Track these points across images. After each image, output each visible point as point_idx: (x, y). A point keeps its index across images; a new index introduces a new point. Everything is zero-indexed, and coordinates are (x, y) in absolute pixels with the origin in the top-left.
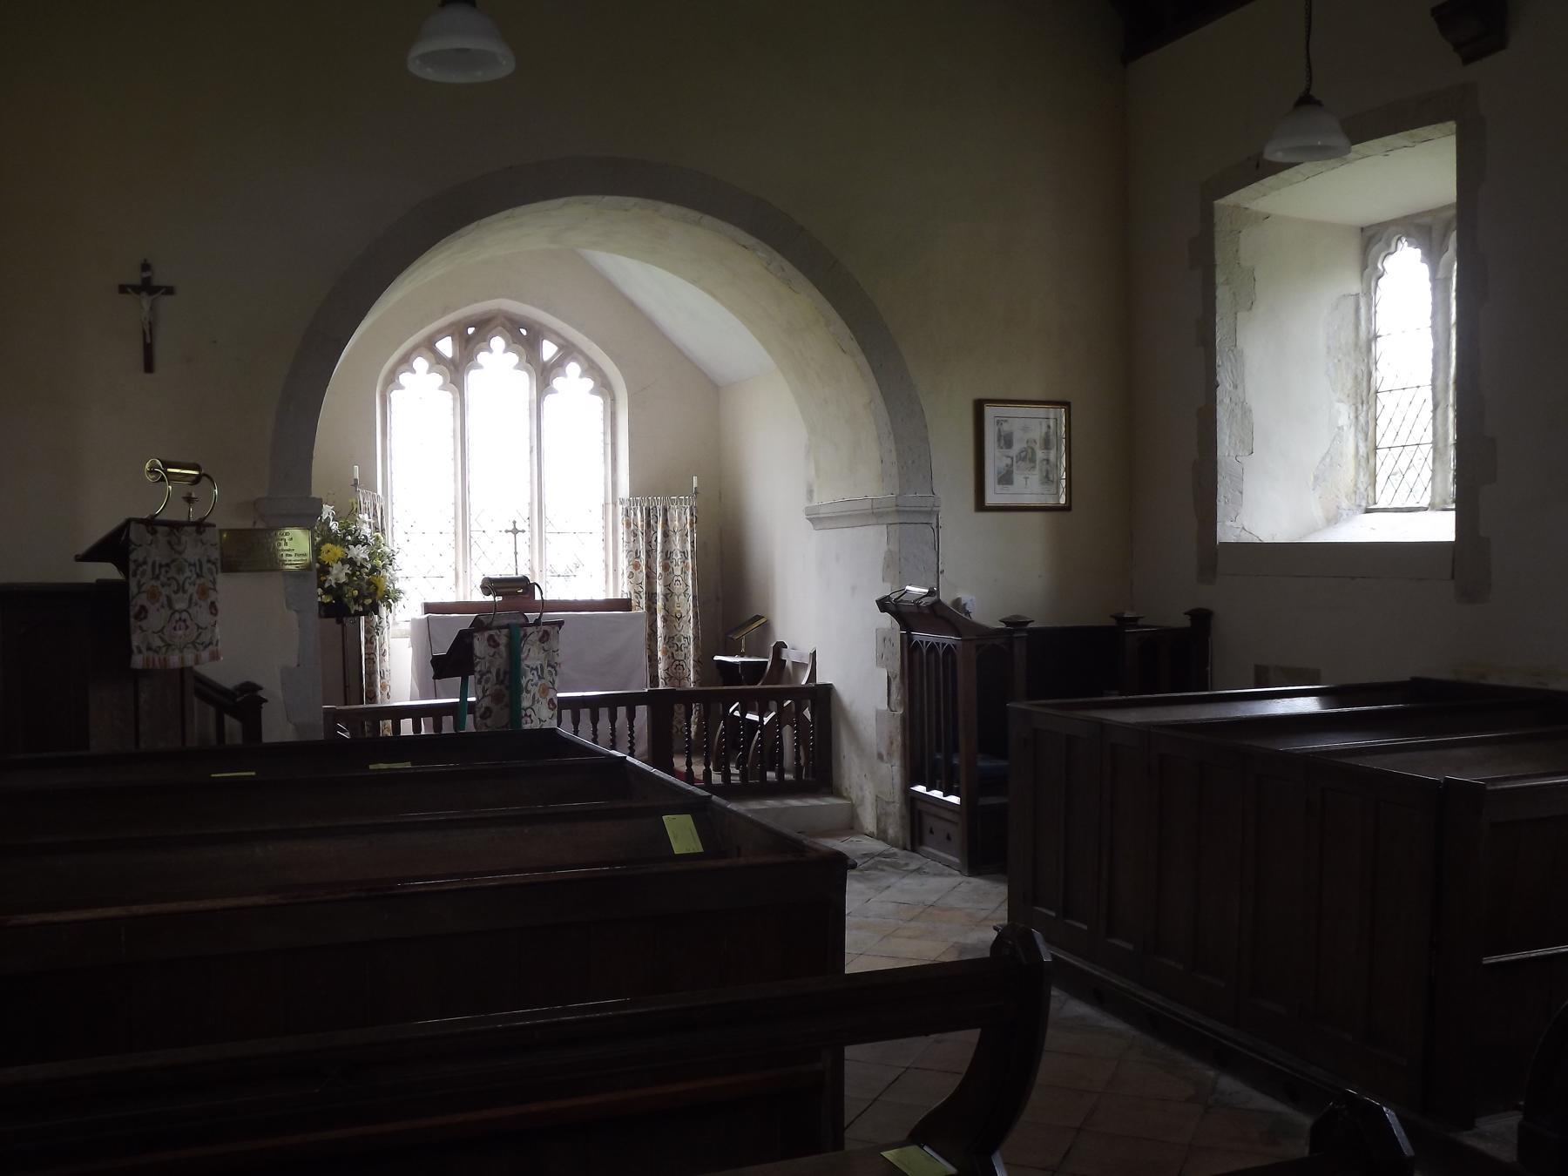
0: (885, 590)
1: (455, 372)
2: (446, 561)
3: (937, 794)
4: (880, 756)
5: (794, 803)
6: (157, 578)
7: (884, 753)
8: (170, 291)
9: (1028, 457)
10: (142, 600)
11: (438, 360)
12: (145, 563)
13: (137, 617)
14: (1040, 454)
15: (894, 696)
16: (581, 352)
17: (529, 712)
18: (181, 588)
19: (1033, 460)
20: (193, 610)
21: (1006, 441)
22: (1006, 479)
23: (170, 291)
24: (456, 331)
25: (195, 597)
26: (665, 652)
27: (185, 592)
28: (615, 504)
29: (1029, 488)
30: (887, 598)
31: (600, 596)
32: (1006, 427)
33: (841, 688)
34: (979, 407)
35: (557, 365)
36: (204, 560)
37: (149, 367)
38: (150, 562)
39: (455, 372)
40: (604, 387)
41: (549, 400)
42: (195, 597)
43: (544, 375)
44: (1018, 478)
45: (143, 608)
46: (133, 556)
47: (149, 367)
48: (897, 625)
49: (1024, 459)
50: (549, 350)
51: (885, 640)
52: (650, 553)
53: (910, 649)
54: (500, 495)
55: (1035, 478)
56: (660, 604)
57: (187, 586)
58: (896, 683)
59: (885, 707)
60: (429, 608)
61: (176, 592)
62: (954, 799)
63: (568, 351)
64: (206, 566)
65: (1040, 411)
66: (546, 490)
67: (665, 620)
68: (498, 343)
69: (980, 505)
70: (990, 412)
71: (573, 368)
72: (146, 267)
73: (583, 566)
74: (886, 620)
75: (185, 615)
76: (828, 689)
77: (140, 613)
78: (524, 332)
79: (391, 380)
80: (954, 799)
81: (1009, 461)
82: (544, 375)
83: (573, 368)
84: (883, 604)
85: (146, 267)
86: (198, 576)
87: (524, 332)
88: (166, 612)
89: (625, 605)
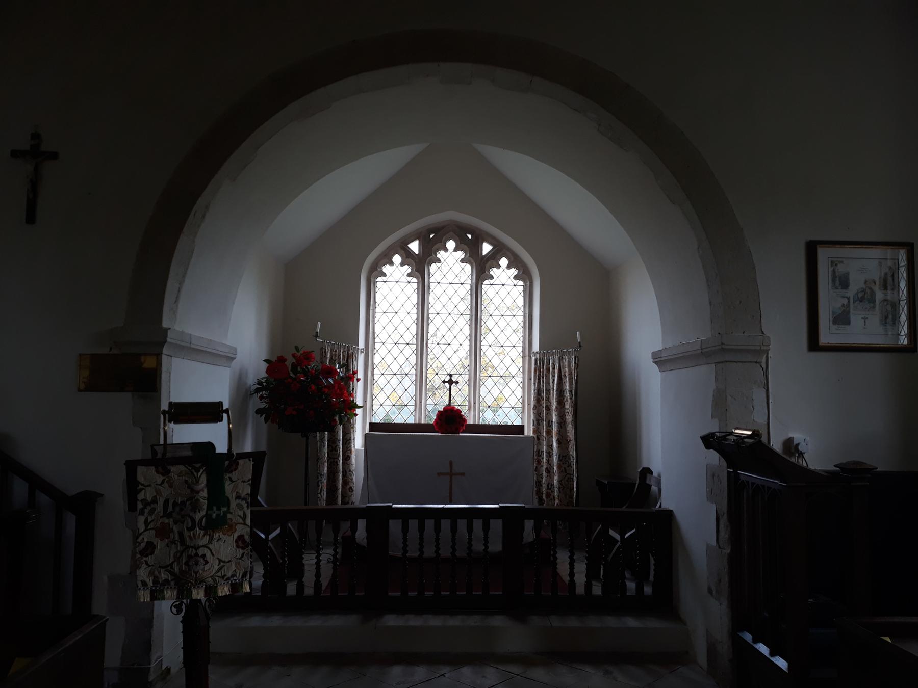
0: (713, 427)
1: (420, 266)
2: (408, 398)
3: (763, 649)
4: (710, 591)
5: (632, 622)
7: (713, 588)
8: (54, 156)
9: (865, 298)
11: (408, 257)
14: (879, 295)
15: (722, 533)
16: (509, 249)
17: (201, 551)
19: (872, 300)
21: (842, 282)
22: (842, 319)
23: (54, 156)
24: (422, 236)
26: (559, 467)
28: (530, 357)
29: (864, 329)
30: (712, 435)
31: (411, 420)
32: (841, 269)
33: (680, 516)
34: (811, 248)
35: (493, 259)
37: (31, 218)
39: (420, 266)
40: (524, 275)
41: (486, 286)
43: (482, 269)
44: (856, 319)
46: (141, 496)
47: (31, 218)
48: (725, 464)
49: (861, 300)
50: (487, 248)
51: (712, 475)
53: (735, 486)
54: (449, 351)
55: (875, 319)
56: (555, 429)
58: (724, 521)
59: (714, 543)
60: (374, 427)
62: (781, 663)
63: (499, 250)
65: (875, 253)
66: (765, 400)
67: (559, 442)
68: (451, 244)
69: (814, 344)
70: (823, 254)
71: (504, 262)
72: (36, 136)
73: (504, 399)
74: (714, 457)
76: (669, 514)
78: (470, 236)
79: (376, 271)
80: (781, 663)
81: (845, 301)
82: (482, 269)
83: (504, 262)
84: (709, 441)
87: (470, 236)
89: (520, 429)
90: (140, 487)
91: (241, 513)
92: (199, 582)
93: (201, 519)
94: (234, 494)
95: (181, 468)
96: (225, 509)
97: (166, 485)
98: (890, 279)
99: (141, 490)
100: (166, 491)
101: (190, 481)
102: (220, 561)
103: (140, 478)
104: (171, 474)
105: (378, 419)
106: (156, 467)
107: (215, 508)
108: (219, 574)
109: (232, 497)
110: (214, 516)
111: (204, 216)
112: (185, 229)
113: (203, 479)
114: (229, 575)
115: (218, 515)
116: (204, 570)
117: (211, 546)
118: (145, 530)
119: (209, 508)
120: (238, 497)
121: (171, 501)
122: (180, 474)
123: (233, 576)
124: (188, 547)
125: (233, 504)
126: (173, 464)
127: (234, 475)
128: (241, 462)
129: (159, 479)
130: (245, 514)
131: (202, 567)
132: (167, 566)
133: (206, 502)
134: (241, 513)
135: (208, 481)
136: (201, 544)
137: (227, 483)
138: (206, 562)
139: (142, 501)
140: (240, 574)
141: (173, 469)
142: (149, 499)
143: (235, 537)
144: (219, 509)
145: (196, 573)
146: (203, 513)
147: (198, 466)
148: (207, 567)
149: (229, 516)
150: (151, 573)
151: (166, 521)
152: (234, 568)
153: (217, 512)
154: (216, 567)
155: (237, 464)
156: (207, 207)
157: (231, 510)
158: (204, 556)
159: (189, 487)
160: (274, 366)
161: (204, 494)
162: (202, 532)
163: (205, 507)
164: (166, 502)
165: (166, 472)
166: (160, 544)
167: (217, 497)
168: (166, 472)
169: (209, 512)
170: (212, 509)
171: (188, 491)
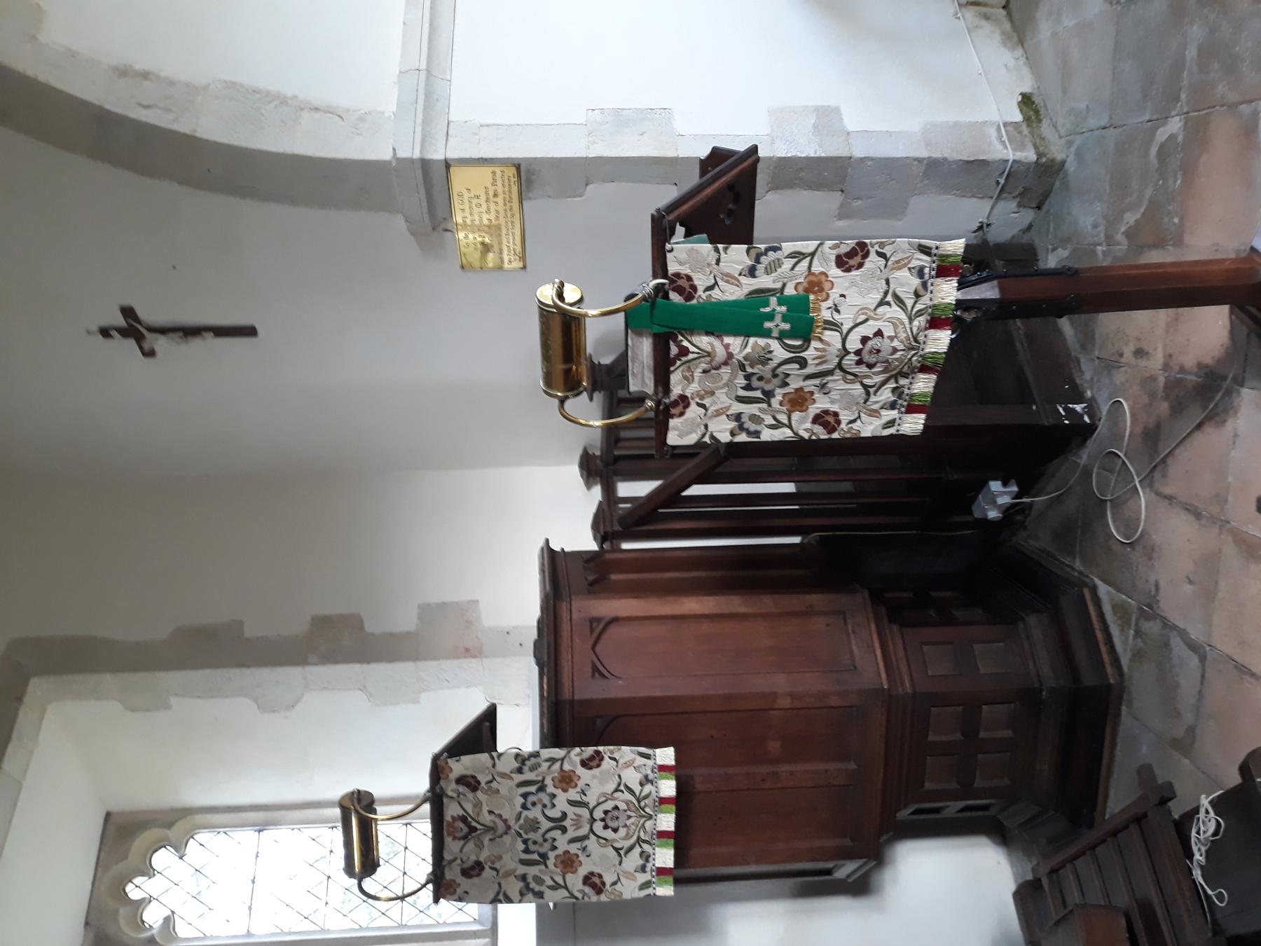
6: (544, 857)
10: (575, 881)
12: (524, 878)
13: (599, 890)
17: (854, 343)
18: (559, 823)
20: (591, 799)
25: (573, 794)
36: (519, 778)
37: (250, 331)
38: (522, 870)
42: (573, 794)
45: (587, 880)
46: (725, 438)
47: (250, 331)
52: (510, 192)
57: (555, 813)
61: (564, 830)
64: (529, 776)
75: (598, 814)
77: (593, 886)
85: (105, 332)
88: (837, 383)
90: (707, 439)
91: (788, 264)
92: (915, 343)
93: (788, 348)
94: (743, 280)
95: (676, 378)
96: (773, 300)
97: (707, 402)
98: (983, 9)
99: (712, 437)
100: (722, 399)
101: (704, 366)
102: (882, 303)
103: (691, 439)
104: (688, 393)
105: (659, 762)
106: (672, 416)
107: (768, 325)
108: (909, 303)
109: (749, 284)
110: (787, 326)
111: (145, 75)
112: (183, 127)
113: (704, 341)
114: (916, 282)
115: (785, 318)
116: (891, 338)
117: (845, 328)
118: (790, 427)
119: (767, 334)
120: (752, 272)
121: (742, 393)
122: (688, 379)
123: (920, 273)
124: (839, 366)
125: (764, 281)
126: (667, 390)
127: (701, 281)
128: (673, 268)
129: (693, 411)
130: (791, 256)
131: (886, 341)
132: (868, 394)
133: (752, 340)
134: (788, 264)
135: (708, 333)
136: (839, 346)
137: (716, 294)
138: (879, 333)
139: (733, 434)
140: (922, 260)
141: (676, 391)
142: (733, 424)
143: (839, 272)
144: (771, 317)
145: (895, 350)
146: (775, 345)
147: (674, 350)
148: (888, 331)
149: (790, 291)
150: (874, 413)
151: (779, 398)
152: (904, 274)
153: (778, 318)
154: (895, 311)
155: (678, 275)
156: (124, 72)
157: (778, 285)
158: (865, 340)
159: (718, 368)
161: (734, 342)
162: (814, 344)
163: (762, 342)
164: (524, 862)
165: (684, 401)
166: (821, 403)
167: (744, 318)
168: (684, 401)
169: (775, 334)
170: (770, 330)
171: (726, 371)
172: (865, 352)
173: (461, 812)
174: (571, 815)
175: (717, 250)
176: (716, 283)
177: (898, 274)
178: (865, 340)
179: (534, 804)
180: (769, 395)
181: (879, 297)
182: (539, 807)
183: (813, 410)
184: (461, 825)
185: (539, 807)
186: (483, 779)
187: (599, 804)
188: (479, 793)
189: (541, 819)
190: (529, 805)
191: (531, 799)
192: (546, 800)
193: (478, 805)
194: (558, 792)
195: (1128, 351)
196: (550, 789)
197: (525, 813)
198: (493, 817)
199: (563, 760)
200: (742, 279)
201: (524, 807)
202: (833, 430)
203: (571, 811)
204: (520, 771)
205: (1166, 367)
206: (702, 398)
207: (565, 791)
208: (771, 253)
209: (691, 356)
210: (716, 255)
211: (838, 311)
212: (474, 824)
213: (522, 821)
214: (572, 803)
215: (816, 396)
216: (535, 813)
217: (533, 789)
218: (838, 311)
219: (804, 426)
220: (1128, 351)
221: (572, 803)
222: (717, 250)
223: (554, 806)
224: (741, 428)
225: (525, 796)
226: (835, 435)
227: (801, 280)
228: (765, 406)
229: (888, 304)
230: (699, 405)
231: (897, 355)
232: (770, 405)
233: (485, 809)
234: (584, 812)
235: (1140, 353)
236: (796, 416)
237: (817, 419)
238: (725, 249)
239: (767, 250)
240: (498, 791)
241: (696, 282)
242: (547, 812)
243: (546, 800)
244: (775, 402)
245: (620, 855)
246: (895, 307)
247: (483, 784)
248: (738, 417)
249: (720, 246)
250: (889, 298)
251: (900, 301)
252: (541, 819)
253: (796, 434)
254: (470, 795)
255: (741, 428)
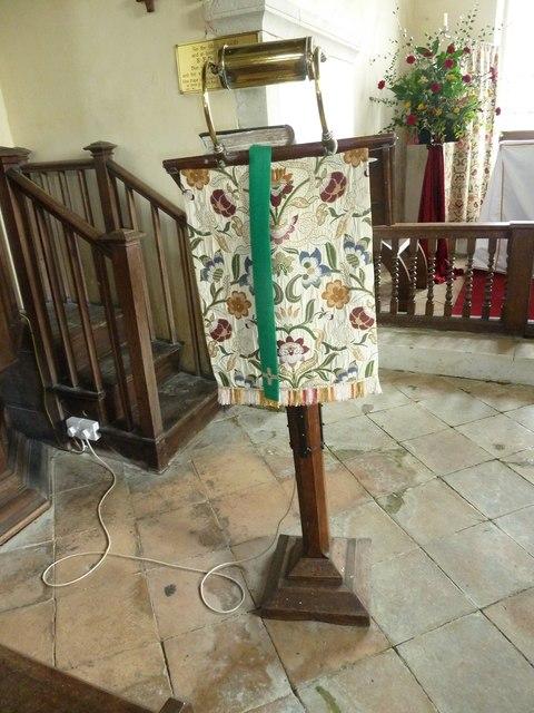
8: (202, 135)
12: (219, 260)
23: (202, 135)
25: (320, 304)
27: (293, 299)
36: (338, 245)
42: (320, 304)
46: (198, 252)
57: (298, 289)
60: (506, 136)
64: (341, 255)
75: (296, 335)
86: (325, 270)
104: (237, 213)
117: (310, 326)
118: (214, 303)
130: (362, 273)
131: (300, 356)
138: (306, 349)
148: (308, 356)
160: (247, 151)
172: (290, 344)
173: (295, 185)
174: (296, 306)
175: (365, 213)
176: (337, 217)
177: (351, 355)
178: (300, 341)
179: (307, 265)
180: (243, 281)
181: (333, 344)
182: (304, 271)
183: (231, 319)
184: (282, 187)
185: (304, 271)
186: (338, 205)
187: (310, 332)
188: (320, 201)
189: (291, 276)
190: (306, 260)
191: (313, 261)
192: (312, 278)
193: (306, 202)
194: (322, 289)
195: (208, 476)
196: (326, 280)
197: (297, 257)
198: (290, 222)
199: (363, 289)
200: (342, 237)
201: (304, 255)
202: (214, 335)
203: (301, 306)
204: (348, 244)
205: (212, 501)
206: (235, 226)
207: (324, 296)
208: (363, 257)
209: (273, 208)
210: (361, 212)
211: (321, 316)
212: (283, 201)
213: (287, 255)
214: (311, 305)
215: (244, 318)
216: (298, 267)
217: (325, 261)
218: (321, 316)
219: (214, 314)
220: (208, 476)
221: (311, 305)
222: (365, 213)
223: (306, 287)
224: (209, 264)
225: (317, 254)
226: (209, 339)
227: (343, 284)
228: (232, 280)
229: (328, 352)
230: (228, 224)
231: (289, 369)
232: (232, 284)
233: (300, 212)
234: (300, 319)
235: (211, 483)
236: (224, 306)
237: (223, 323)
238: (366, 220)
239: (366, 254)
240: (320, 223)
241: (338, 200)
242: (300, 280)
243: (312, 278)
244: (236, 287)
245: (250, 356)
246: (325, 357)
247: (330, 205)
248: (219, 260)
249: (369, 216)
250: (331, 352)
251: (329, 361)
252: (291, 276)
253: (207, 310)
254: (317, 192)
255: (209, 264)
